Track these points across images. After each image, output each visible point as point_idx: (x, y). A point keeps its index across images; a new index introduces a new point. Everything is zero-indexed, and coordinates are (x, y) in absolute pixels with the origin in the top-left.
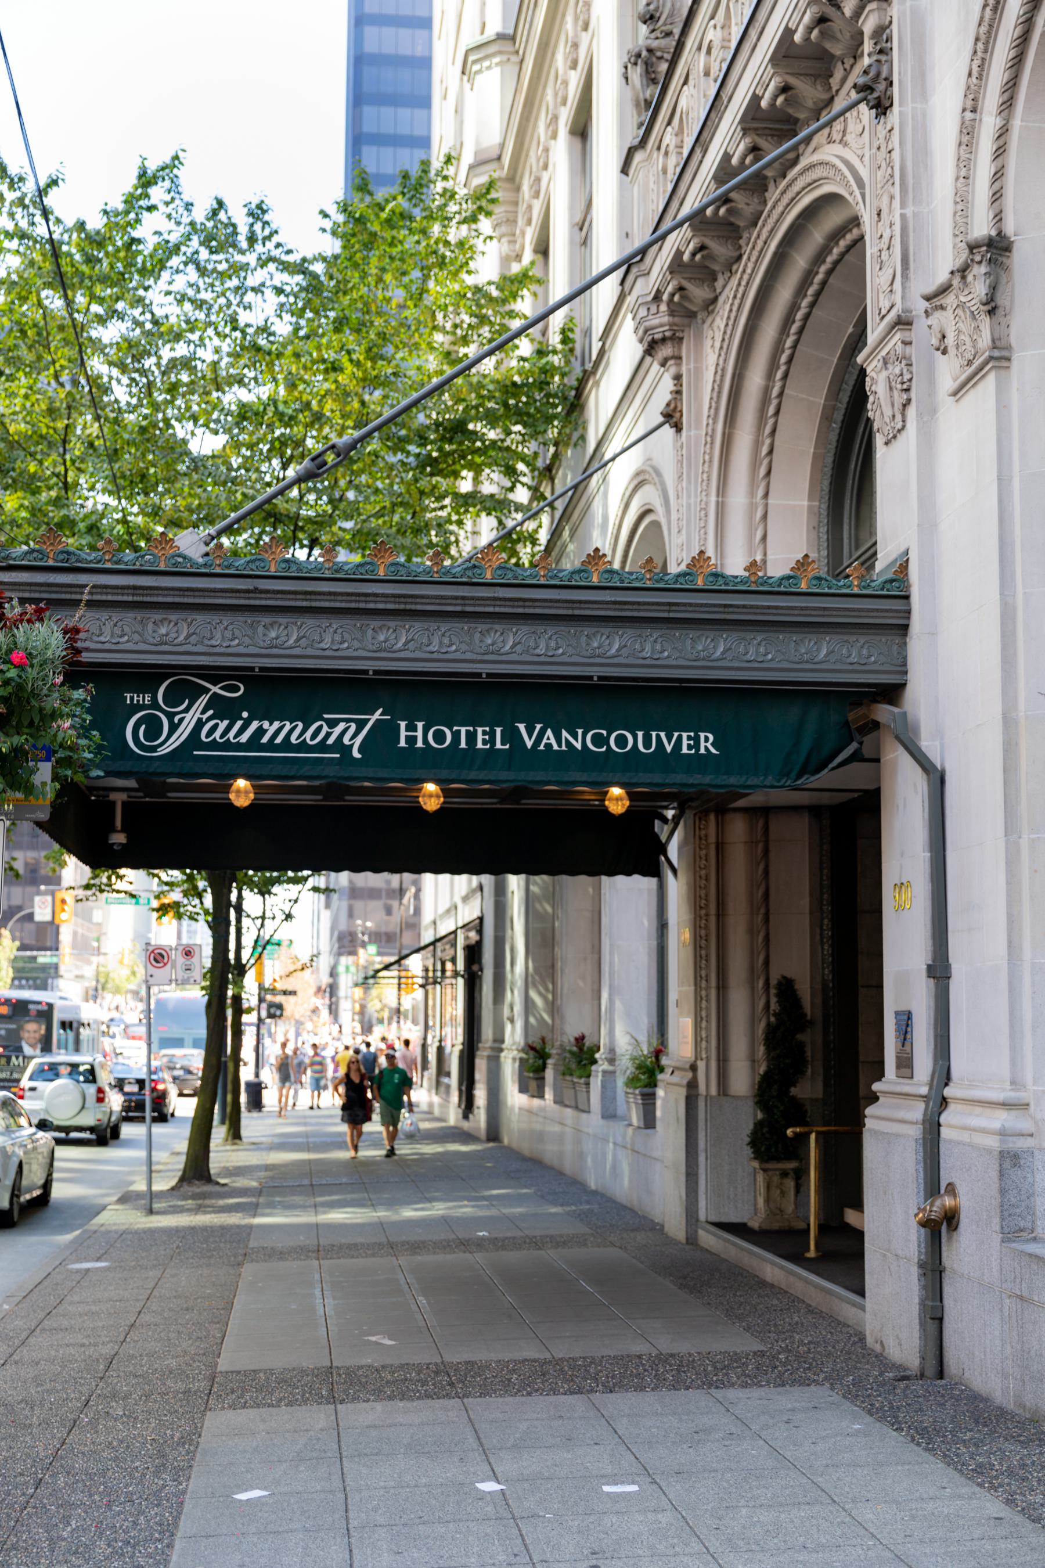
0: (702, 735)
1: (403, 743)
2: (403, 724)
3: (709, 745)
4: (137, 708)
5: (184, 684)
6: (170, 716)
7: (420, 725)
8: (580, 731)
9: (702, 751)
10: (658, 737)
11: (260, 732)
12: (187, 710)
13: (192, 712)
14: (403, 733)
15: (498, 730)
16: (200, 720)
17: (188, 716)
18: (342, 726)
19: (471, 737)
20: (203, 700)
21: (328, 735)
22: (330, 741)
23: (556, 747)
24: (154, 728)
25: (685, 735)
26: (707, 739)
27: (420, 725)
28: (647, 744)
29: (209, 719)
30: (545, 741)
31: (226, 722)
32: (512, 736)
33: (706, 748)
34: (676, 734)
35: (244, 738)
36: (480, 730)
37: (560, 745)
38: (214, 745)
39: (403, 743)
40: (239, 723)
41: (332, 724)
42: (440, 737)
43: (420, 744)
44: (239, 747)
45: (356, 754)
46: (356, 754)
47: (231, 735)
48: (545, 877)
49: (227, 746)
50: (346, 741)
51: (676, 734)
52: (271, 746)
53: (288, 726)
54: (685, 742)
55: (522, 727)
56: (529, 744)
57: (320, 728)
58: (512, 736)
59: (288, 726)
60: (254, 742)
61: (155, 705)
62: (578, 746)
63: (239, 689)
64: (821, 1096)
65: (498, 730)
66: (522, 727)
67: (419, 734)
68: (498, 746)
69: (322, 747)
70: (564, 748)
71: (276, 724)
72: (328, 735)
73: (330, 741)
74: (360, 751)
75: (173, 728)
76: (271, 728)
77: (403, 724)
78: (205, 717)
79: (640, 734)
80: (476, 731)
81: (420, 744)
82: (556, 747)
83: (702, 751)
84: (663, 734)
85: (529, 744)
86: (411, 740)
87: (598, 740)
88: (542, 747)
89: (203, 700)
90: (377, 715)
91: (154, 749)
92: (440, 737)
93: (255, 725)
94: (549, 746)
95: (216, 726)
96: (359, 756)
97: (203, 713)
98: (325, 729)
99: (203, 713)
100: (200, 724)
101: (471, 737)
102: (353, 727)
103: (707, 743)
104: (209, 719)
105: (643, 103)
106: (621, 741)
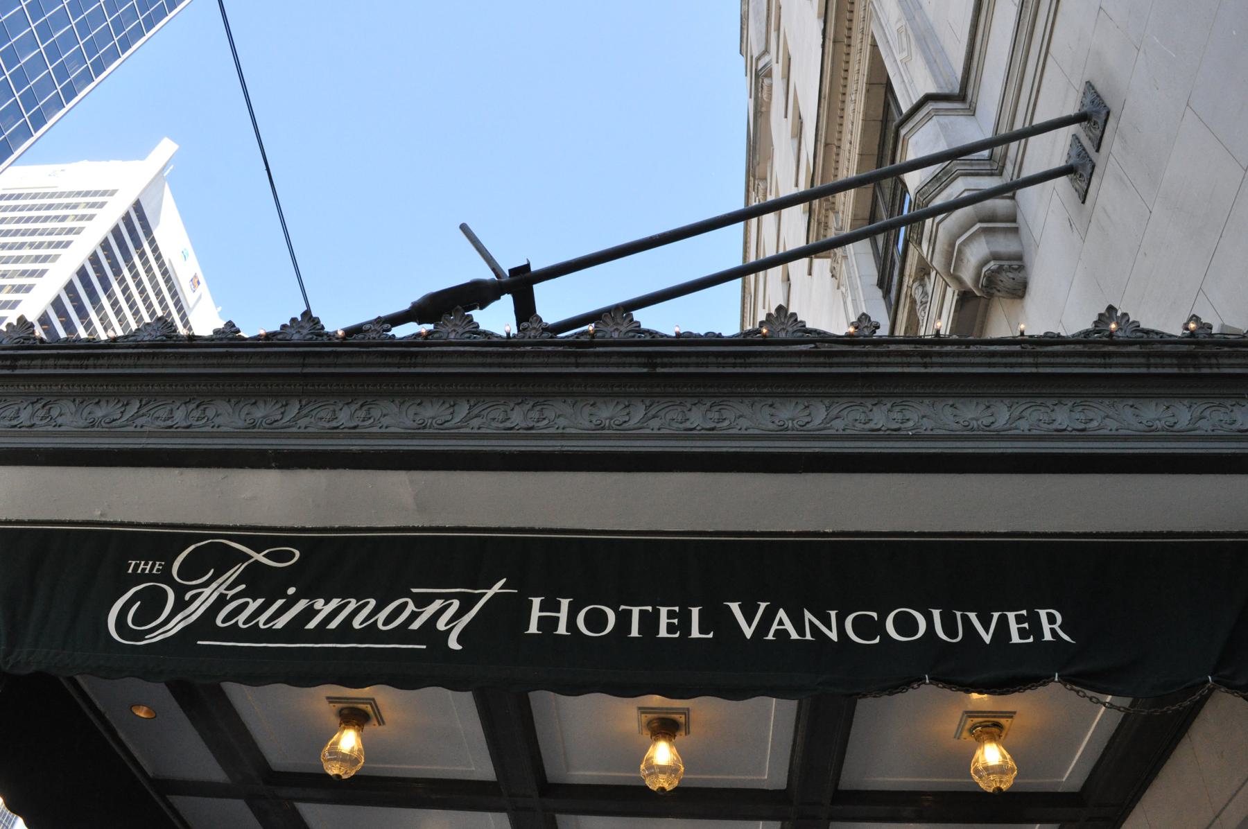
0: (1043, 614)
1: (533, 628)
2: (536, 602)
3: (1056, 626)
4: (138, 578)
5: (211, 552)
6: (180, 591)
7: (565, 603)
8: (833, 614)
9: (1048, 636)
10: (966, 620)
11: (310, 613)
12: (206, 584)
13: (214, 585)
14: (536, 614)
15: (695, 612)
16: (222, 596)
17: (207, 591)
18: (438, 604)
19: (649, 622)
20: (238, 570)
21: (414, 616)
22: (415, 625)
23: (794, 635)
24: (151, 605)
25: (1011, 616)
26: (1052, 619)
27: (565, 603)
28: (950, 629)
29: (234, 597)
30: (775, 627)
31: (260, 601)
32: (717, 619)
33: (1053, 631)
34: (996, 615)
35: (280, 623)
36: (664, 611)
37: (801, 631)
38: (233, 633)
39: (533, 628)
40: (280, 602)
41: (423, 601)
42: (596, 621)
43: (562, 629)
44: (271, 635)
45: (453, 644)
46: (453, 644)
47: (262, 619)
48: (654, 787)
49: (254, 633)
50: (441, 625)
51: (996, 615)
52: (321, 632)
53: (353, 604)
54: (1014, 627)
55: (735, 607)
56: (748, 632)
57: (405, 605)
58: (717, 619)
59: (353, 604)
60: (296, 629)
61: (166, 576)
62: (833, 636)
63: (293, 555)
64: (535, 287)
65: (695, 612)
66: (735, 607)
67: (563, 615)
68: (695, 633)
69: (402, 633)
70: (808, 637)
71: (335, 603)
72: (414, 616)
73: (415, 625)
74: (459, 640)
75: (180, 605)
76: (324, 608)
77: (536, 602)
78: (231, 593)
79: (936, 614)
80: (656, 614)
81: (562, 629)
82: (794, 635)
83: (1048, 636)
84: (973, 616)
85: (748, 632)
86: (548, 624)
87: (862, 627)
88: (770, 637)
89: (238, 570)
90: (496, 588)
91: (141, 635)
92: (596, 621)
93: (302, 604)
94: (781, 634)
95: (246, 605)
96: (460, 647)
97: (229, 588)
98: (411, 607)
99: (229, 588)
100: (222, 601)
101: (649, 622)
102: (456, 604)
103: (1050, 625)
104: (234, 597)
105: (990, 411)
106: (907, 625)
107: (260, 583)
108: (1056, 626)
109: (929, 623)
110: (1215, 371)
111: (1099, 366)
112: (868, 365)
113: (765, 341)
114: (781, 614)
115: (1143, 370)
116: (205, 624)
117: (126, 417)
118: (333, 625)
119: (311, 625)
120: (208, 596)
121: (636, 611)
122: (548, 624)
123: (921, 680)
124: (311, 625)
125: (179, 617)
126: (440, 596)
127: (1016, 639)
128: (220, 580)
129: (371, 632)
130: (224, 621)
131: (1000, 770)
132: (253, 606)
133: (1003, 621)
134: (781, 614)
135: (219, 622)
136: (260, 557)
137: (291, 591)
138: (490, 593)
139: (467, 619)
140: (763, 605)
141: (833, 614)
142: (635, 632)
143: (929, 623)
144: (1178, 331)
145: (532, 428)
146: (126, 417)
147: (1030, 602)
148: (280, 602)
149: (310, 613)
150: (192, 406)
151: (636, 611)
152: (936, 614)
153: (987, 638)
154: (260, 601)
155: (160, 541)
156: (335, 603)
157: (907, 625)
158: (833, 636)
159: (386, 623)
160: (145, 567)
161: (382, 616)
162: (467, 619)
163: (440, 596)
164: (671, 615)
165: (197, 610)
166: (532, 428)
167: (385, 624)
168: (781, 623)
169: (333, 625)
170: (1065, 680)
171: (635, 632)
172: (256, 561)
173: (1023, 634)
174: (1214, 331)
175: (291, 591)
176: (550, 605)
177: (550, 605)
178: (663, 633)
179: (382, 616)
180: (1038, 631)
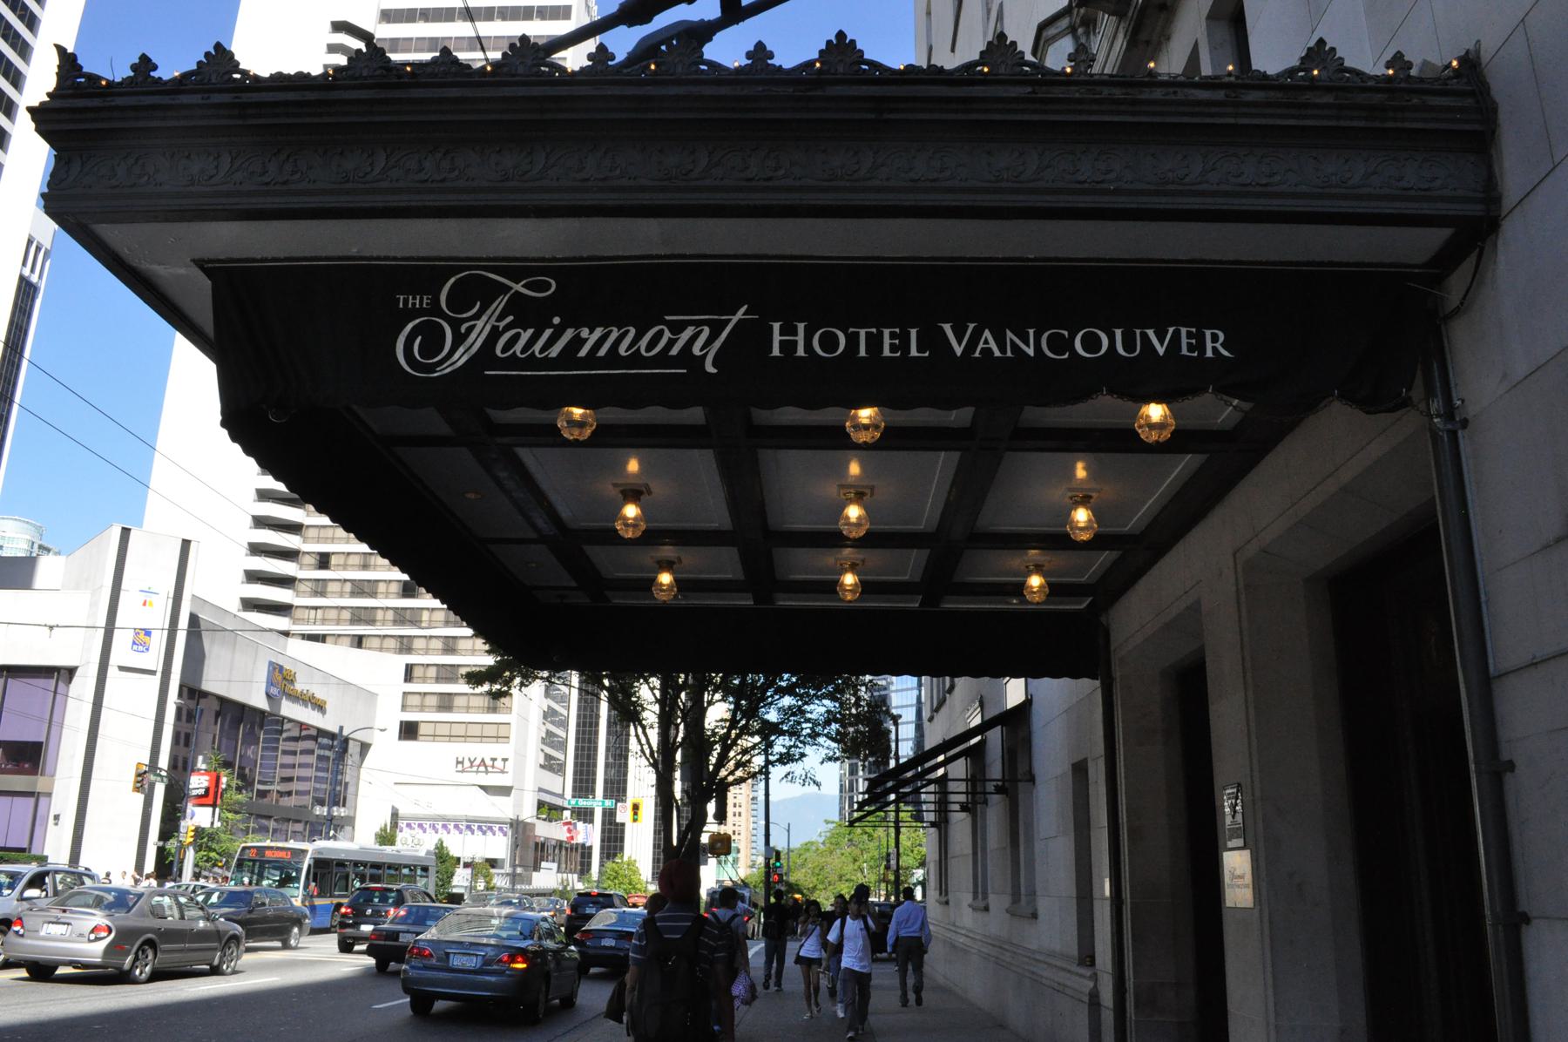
0: (1208, 333)
1: (776, 352)
2: (776, 326)
3: (1218, 345)
6: (455, 325)
7: (801, 327)
8: (1031, 332)
9: (1209, 354)
10: (1145, 337)
12: (477, 317)
13: (484, 318)
14: (777, 338)
15: (913, 332)
16: (494, 328)
17: (480, 324)
18: (689, 332)
19: (875, 343)
20: (500, 303)
21: (671, 343)
22: (674, 351)
23: (997, 353)
24: (433, 341)
25: (1184, 331)
26: (1215, 338)
27: (801, 327)
28: (1129, 346)
30: (981, 345)
31: (530, 331)
32: (933, 339)
34: (1171, 330)
35: (554, 352)
36: (886, 332)
37: (1003, 349)
38: (513, 362)
39: (776, 352)
40: (548, 332)
41: (677, 328)
42: (829, 342)
43: (801, 352)
44: (548, 363)
46: (710, 368)
47: (537, 347)
50: (696, 350)
51: (1171, 330)
55: (947, 328)
56: (959, 350)
57: (661, 333)
58: (933, 339)
61: (435, 309)
62: (1031, 352)
65: (913, 332)
66: (947, 328)
67: (800, 338)
68: (914, 352)
69: (663, 359)
70: (1009, 354)
71: (599, 332)
72: (671, 343)
73: (674, 351)
74: (714, 364)
75: (459, 339)
77: (776, 326)
78: (502, 324)
79: (1118, 333)
80: (881, 334)
81: (801, 352)
82: (997, 353)
83: (1209, 354)
84: (1151, 333)
85: (959, 350)
86: (789, 347)
87: (1058, 344)
88: (977, 355)
89: (500, 303)
90: (740, 314)
91: (432, 368)
92: (829, 342)
93: (569, 334)
94: (987, 352)
97: (500, 319)
98: (667, 334)
99: (500, 319)
100: (495, 334)
101: (875, 343)
102: (706, 331)
103: (1214, 344)
106: (1091, 343)
107: (525, 313)
108: (1218, 345)
109: (1112, 341)
110: (1399, 125)
111: (1293, 117)
112: (1080, 112)
113: (985, 80)
114: (987, 333)
115: (1333, 123)
116: (485, 355)
117: (377, 170)
118: (602, 352)
119: (583, 353)
120: (480, 331)
121: (863, 332)
122: (789, 347)
123: (1099, 391)
124: (583, 353)
125: (461, 350)
126: (691, 323)
127: (1185, 351)
128: (489, 312)
129: (635, 359)
130: (503, 351)
131: (1160, 426)
132: (526, 335)
133: (1177, 334)
134: (987, 333)
135: (498, 352)
136: (519, 287)
137: (556, 320)
138: (735, 319)
139: (717, 344)
140: (972, 326)
141: (1031, 332)
142: (862, 353)
143: (1112, 341)
144: (1379, 70)
145: (769, 179)
146: (377, 170)
147: (1201, 323)
148: (548, 332)
149: (578, 342)
150: (438, 156)
151: (863, 332)
152: (1118, 333)
153: (1161, 351)
154: (530, 331)
155: (424, 275)
156: (599, 332)
157: (1091, 343)
158: (1031, 352)
159: (649, 349)
160: (415, 302)
161: (644, 343)
162: (717, 344)
163: (691, 323)
164: (893, 336)
165: (476, 340)
166: (769, 179)
167: (648, 350)
168: (986, 342)
169: (602, 352)
170: (1217, 391)
171: (862, 353)
172: (517, 292)
173: (1191, 348)
174: (1413, 72)
175: (556, 320)
176: (789, 329)
177: (789, 329)
178: (887, 352)
179: (644, 343)
180: (1203, 349)
